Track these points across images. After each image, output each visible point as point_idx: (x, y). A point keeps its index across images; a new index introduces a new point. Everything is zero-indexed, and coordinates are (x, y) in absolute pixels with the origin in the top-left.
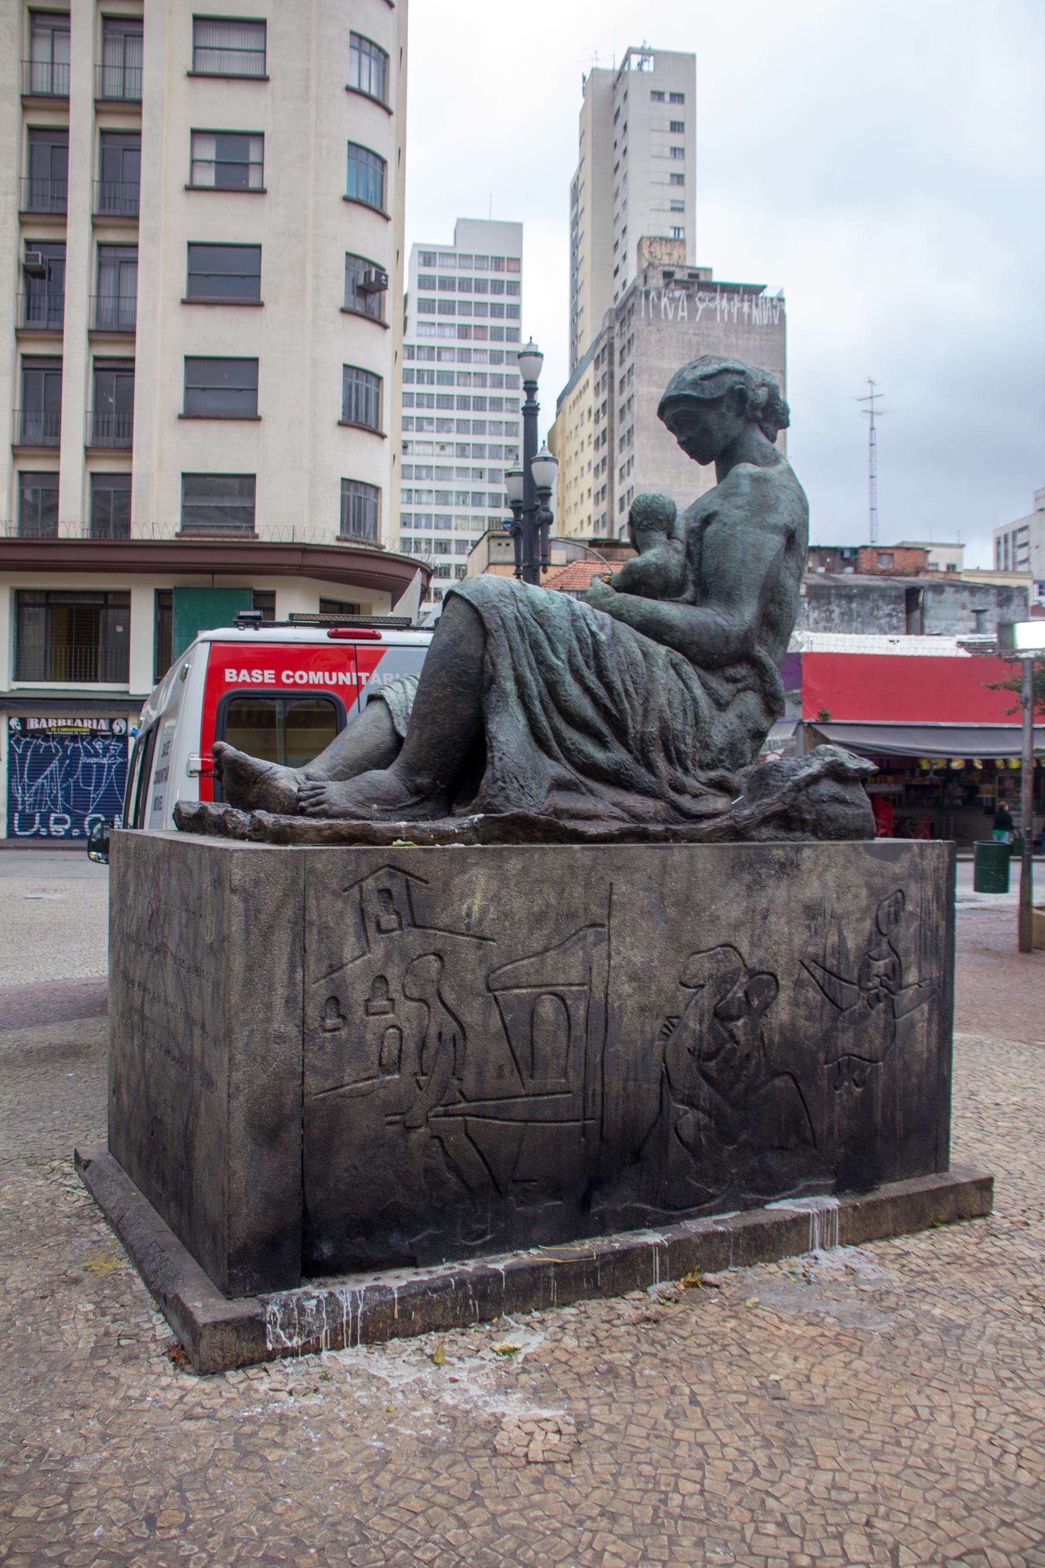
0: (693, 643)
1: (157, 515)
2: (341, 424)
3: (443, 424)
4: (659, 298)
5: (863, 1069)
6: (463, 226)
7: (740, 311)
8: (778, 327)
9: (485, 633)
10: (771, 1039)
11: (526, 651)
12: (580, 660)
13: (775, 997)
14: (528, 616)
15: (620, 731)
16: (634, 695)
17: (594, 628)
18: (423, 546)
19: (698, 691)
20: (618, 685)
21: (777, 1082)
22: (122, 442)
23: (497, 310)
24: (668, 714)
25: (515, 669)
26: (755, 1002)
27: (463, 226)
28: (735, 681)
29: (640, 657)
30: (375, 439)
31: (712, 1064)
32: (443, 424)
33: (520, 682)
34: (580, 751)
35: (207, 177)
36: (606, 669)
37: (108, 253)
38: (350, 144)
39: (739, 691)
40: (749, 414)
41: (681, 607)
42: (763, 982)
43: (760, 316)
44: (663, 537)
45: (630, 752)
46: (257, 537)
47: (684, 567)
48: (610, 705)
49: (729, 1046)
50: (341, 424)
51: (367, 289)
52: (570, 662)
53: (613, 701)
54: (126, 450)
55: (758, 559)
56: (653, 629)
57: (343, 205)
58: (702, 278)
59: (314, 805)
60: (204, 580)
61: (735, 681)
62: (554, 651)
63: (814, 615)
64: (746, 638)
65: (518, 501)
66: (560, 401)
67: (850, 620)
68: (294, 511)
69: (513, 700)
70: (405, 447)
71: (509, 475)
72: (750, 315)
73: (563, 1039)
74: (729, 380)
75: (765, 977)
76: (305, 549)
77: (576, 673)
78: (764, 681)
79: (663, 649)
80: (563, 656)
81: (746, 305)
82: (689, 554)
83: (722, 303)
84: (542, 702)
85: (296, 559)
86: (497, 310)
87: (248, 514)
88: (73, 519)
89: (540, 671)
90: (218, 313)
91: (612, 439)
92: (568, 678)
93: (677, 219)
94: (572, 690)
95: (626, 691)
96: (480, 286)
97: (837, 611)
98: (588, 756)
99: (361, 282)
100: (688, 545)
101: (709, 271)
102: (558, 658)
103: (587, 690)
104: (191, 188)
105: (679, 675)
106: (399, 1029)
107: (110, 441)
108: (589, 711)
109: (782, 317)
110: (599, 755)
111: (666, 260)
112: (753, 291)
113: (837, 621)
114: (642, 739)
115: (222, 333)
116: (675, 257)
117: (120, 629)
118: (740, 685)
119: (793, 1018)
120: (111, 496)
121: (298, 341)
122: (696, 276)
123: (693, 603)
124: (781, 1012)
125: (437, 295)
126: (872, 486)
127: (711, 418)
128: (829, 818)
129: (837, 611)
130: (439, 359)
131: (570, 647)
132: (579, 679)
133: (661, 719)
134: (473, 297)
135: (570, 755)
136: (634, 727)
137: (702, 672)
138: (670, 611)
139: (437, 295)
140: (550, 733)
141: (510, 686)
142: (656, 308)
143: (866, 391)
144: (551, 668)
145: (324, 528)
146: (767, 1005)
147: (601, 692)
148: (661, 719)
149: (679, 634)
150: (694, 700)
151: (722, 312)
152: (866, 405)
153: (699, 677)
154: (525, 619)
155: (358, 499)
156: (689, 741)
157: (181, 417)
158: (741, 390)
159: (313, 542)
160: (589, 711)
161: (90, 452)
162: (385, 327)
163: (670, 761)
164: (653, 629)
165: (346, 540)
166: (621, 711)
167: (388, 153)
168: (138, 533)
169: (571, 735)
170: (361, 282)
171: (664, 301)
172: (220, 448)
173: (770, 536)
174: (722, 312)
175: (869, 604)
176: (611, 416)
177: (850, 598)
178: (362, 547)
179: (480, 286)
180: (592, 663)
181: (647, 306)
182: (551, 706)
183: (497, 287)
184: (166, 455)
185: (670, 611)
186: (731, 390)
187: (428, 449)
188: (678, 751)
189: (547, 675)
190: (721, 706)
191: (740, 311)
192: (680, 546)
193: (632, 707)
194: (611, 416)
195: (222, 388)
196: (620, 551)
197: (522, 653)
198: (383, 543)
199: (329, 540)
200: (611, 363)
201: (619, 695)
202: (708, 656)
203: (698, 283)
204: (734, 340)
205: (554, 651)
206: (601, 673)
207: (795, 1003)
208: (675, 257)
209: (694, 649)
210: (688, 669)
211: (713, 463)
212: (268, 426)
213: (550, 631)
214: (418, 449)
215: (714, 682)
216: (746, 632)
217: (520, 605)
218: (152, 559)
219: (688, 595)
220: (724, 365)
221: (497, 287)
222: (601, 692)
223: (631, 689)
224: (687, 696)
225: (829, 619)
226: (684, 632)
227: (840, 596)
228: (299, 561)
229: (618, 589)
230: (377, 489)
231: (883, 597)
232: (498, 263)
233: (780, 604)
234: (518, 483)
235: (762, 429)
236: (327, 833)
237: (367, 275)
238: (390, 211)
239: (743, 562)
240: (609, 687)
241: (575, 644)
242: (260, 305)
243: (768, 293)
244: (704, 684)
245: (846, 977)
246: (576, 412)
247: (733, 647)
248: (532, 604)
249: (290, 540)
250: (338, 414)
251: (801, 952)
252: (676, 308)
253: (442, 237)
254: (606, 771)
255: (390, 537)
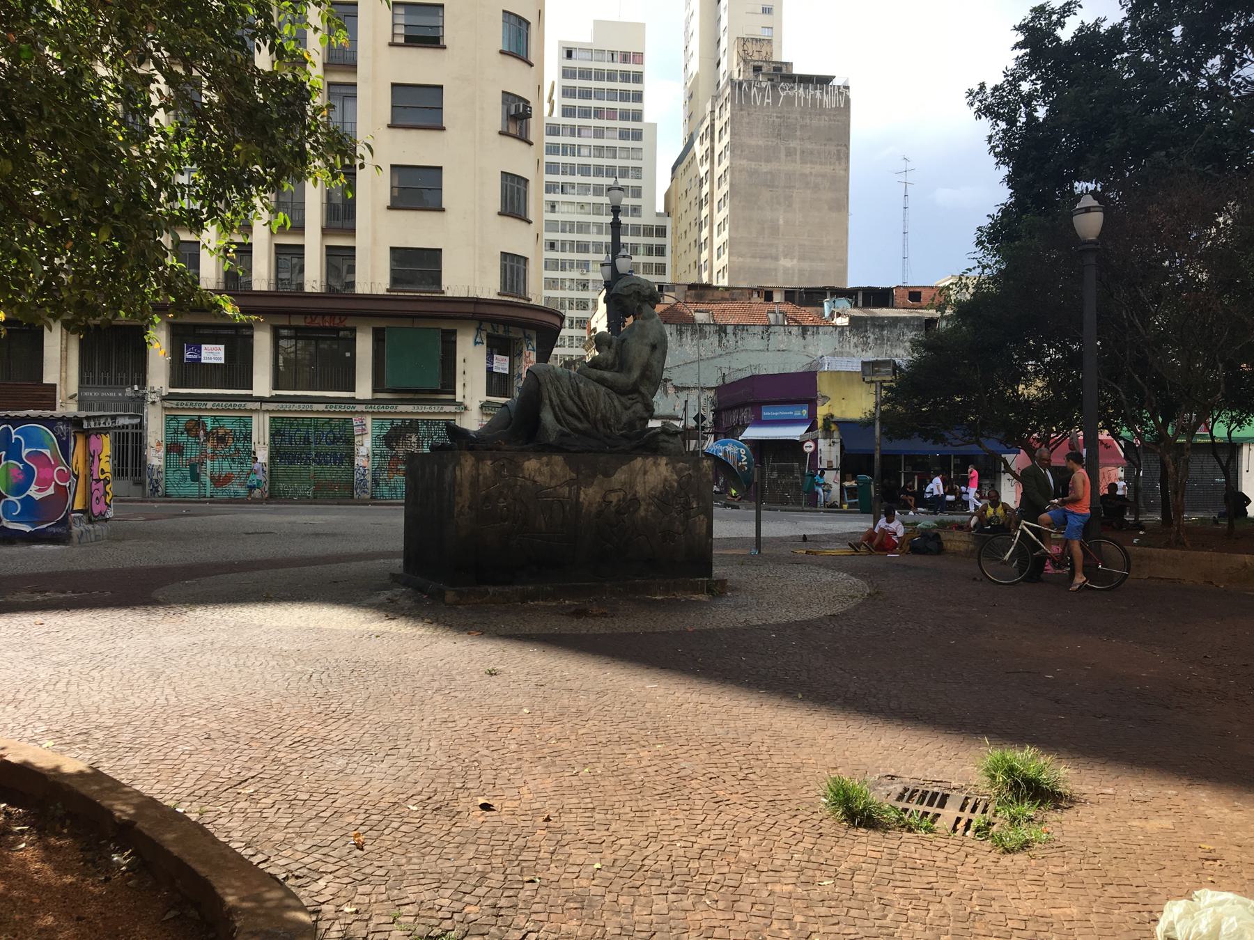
1: (372, 276)
2: (500, 214)
3: (585, 188)
4: (750, 88)
6: (598, 24)
7: (813, 97)
8: (844, 109)
15: (586, 416)
18: (568, 284)
19: (616, 403)
22: (347, 225)
23: (625, 96)
27: (598, 24)
30: (524, 224)
32: (585, 188)
33: (551, 401)
35: (401, 40)
37: (333, 89)
38: (504, 11)
42: (635, 501)
43: (829, 101)
50: (500, 214)
51: (517, 116)
54: (351, 232)
56: (601, 381)
57: (500, 56)
58: (784, 71)
63: (854, 340)
66: (674, 169)
67: (882, 344)
68: (469, 276)
69: (548, 406)
70: (553, 207)
71: (602, 265)
72: (821, 100)
76: (477, 302)
77: (570, 397)
81: (818, 92)
83: (799, 91)
85: (470, 309)
86: (625, 96)
87: (436, 278)
88: (314, 277)
90: (414, 133)
91: (712, 201)
93: (766, 20)
94: (569, 403)
96: (611, 76)
97: (872, 337)
99: (513, 112)
101: (789, 65)
104: (392, 44)
107: (338, 224)
108: (576, 410)
109: (847, 101)
111: (756, 56)
112: (824, 81)
113: (872, 344)
115: (416, 148)
116: (764, 54)
117: (348, 354)
120: (340, 260)
121: (469, 155)
122: (780, 69)
125: (578, 83)
126: (905, 240)
129: (872, 337)
130: (579, 136)
134: (606, 85)
138: (607, 375)
139: (578, 83)
142: (747, 96)
143: (902, 166)
145: (488, 286)
151: (799, 98)
152: (902, 178)
155: (513, 266)
157: (389, 208)
160: (576, 410)
161: (326, 232)
162: (531, 144)
164: (601, 381)
167: (530, 17)
168: (361, 288)
170: (513, 112)
171: (754, 90)
172: (416, 230)
174: (799, 98)
175: (897, 331)
176: (712, 183)
177: (882, 327)
178: (515, 300)
179: (611, 76)
181: (740, 95)
183: (626, 77)
184: (380, 233)
185: (607, 375)
187: (571, 208)
190: (627, 408)
191: (813, 97)
194: (712, 183)
195: (417, 189)
196: (710, 292)
199: (493, 295)
200: (712, 140)
202: (621, 391)
203: (782, 75)
204: (808, 121)
206: (580, 397)
207: (646, 510)
208: (764, 54)
210: (614, 395)
212: (449, 216)
214: (565, 208)
215: (623, 399)
218: (371, 308)
221: (626, 77)
225: (866, 343)
227: (874, 326)
228: (472, 312)
230: (526, 259)
231: (907, 325)
232: (625, 57)
234: (608, 269)
237: (517, 107)
238: (532, 59)
242: (443, 129)
243: (836, 82)
246: (686, 178)
250: (498, 207)
252: (763, 96)
253: (582, 36)
255: (537, 292)
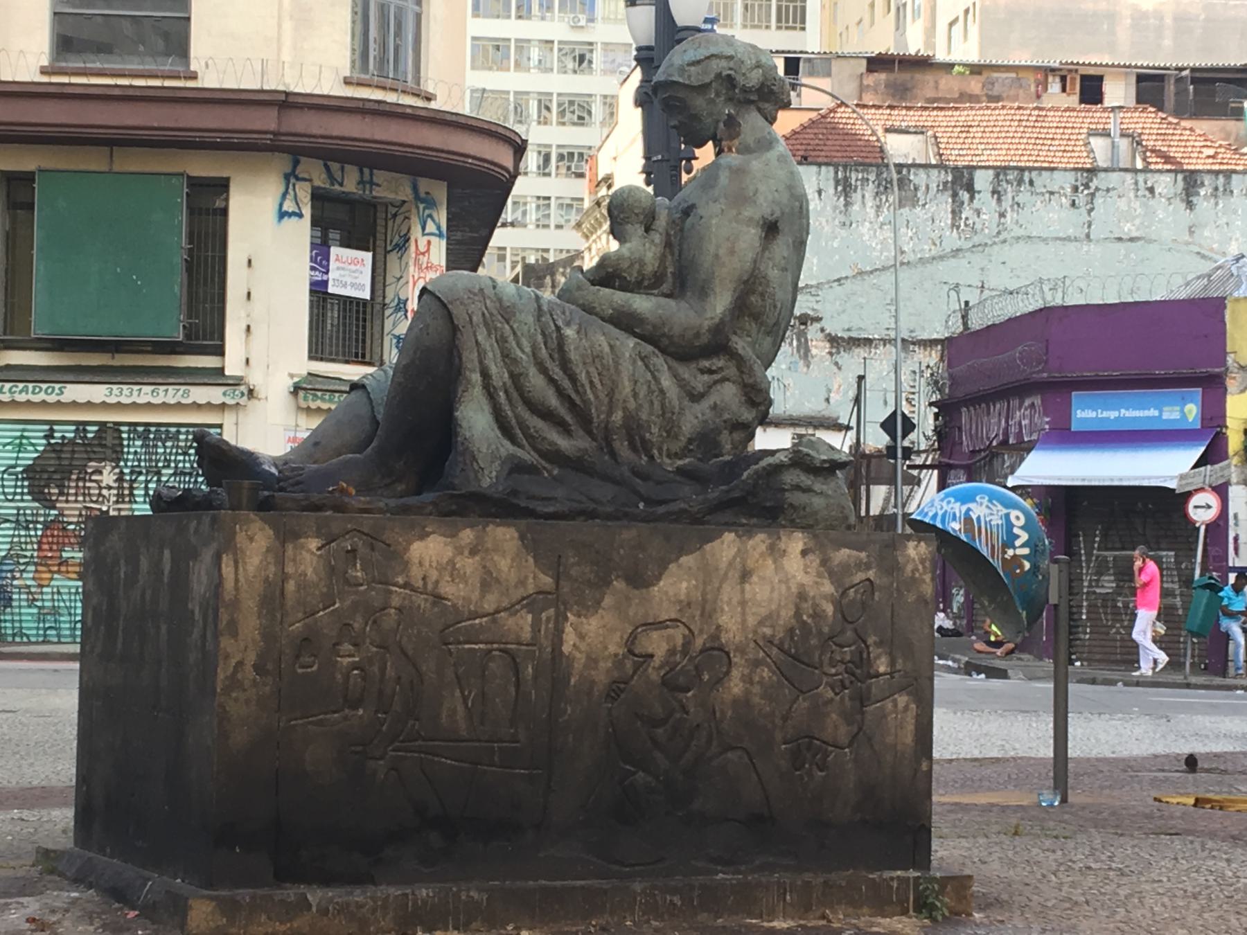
0: (664, 335)
5: (826, 755)
9: (455, 329)
10: (722, 712)
11: (492, 346)
12: (544, 352)
13: (728, 673)
14: (495, 312)
15: (585, 420)
16: (599, 386)
17: (560, 323)
18: (535, 53)
19: (667, 382)
20: (583, 377)
21: (729, 755)
24: (632, 405)
25: (481, 362)
26: (706, 677)
28: (711, 372)
29: (607, 349)
31: (660, 731)
33: (485, 374)
34: (544, 439)
36: (570, 361)
39: (716, 382)
40: (741, 97)
41: (653, 298)
42: (717, 654)
44: (640, 230)
45: (594, 439)
46: (194, 76)
47: (662, 259)
48: (574, 396)
49: (678, 715)
52: (534, 354)
53: (577, 392)
55: (732, 252)
56: (625, 322)
59: (293, 485)
60: (92, 161)
61: (711, 372)
62: (519, 344)
64: (718, 329)
65: (649, 48)
73: (512, 690)
74: (716, 66)
75: (715, 653)
76: (286, 102)
78: (742, 372)
79: (631, 342)
80: (528, 350)
82: (668, 245)
84: (506, 392)
85: (267, 121)
89: (505, 363)
92: (533, 371)
94: (536, 381)
95: (591, 382)
98: (552, 443)
100: (668, 234)
102: (523, 352)
103: (552, 381)
105: (647, 366)
106: (362, 670)
108: (553, 401)
110: (563, 443)
114: (606, 427)
118: (716, 377)
119: (747, 693)
123: (668, 296)
124: (735, 686)
127: (699, 102)
128: (791, 505)
131: (535, 341)
132: (543, 370)
133: (625, 409)
135: (533, 440)
136: (598, 416)
137: (675, 364)
138: (642, 304)
140: (514, 421)
141: (476, 377)
144: (515, 361)
146: (719, 681)
147: (566, 384)
148: (625, 409)
149: (649, 327)
150: (662, 391)
153: (670, 368)
154: (491, 314)
156: (655, 430)
158: (729, 76)
159: (299, 89)
160: (553, 401)
163: (633, 447)
164: (625, 322)
165: (360, 84)
166: (586, 402)
169: (535, 423)
173: (745, 229)
180: (556, 356)
182: (515, 395)
185: (642, 304)
186: (719, 76)
188: (643, 440)
189: (512, 368)
190: (696, 397)
192: (657, 238)
193: (597, 397)
197: (488, 348)
198: (430, 88)
201: (583, 385)
205: (519, 344)
206: (565, 364)
209: (665, 342)
210: (659, 361)
211: (710, 143)
213: (515, 326)
215: (685, 372)
216: (718, 325)
217: (488, 302)
219: (666, 288)
220: (713, 50)
222: (566, 384)
223: (596, 381)
224: (653, 387)
226: (654, 326)
229: (593, 283)
233: (762, 295)
235: (759, 110)
236: (304, 503)
239: (717, 256)
240: (573, 379)
241: (540, 338)
244: (675, 376)
245: (806, 660)
247: (704, 339)
248: (500, 300)
249: (256, 86)
251: (755, 632)
254: (568, 457)
